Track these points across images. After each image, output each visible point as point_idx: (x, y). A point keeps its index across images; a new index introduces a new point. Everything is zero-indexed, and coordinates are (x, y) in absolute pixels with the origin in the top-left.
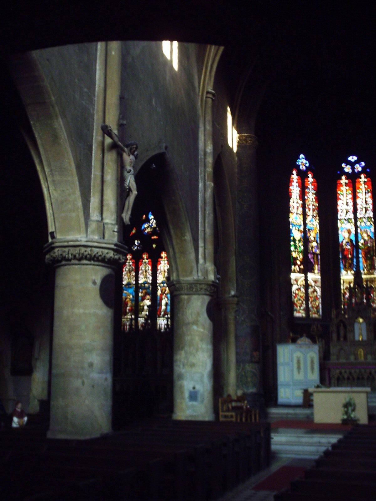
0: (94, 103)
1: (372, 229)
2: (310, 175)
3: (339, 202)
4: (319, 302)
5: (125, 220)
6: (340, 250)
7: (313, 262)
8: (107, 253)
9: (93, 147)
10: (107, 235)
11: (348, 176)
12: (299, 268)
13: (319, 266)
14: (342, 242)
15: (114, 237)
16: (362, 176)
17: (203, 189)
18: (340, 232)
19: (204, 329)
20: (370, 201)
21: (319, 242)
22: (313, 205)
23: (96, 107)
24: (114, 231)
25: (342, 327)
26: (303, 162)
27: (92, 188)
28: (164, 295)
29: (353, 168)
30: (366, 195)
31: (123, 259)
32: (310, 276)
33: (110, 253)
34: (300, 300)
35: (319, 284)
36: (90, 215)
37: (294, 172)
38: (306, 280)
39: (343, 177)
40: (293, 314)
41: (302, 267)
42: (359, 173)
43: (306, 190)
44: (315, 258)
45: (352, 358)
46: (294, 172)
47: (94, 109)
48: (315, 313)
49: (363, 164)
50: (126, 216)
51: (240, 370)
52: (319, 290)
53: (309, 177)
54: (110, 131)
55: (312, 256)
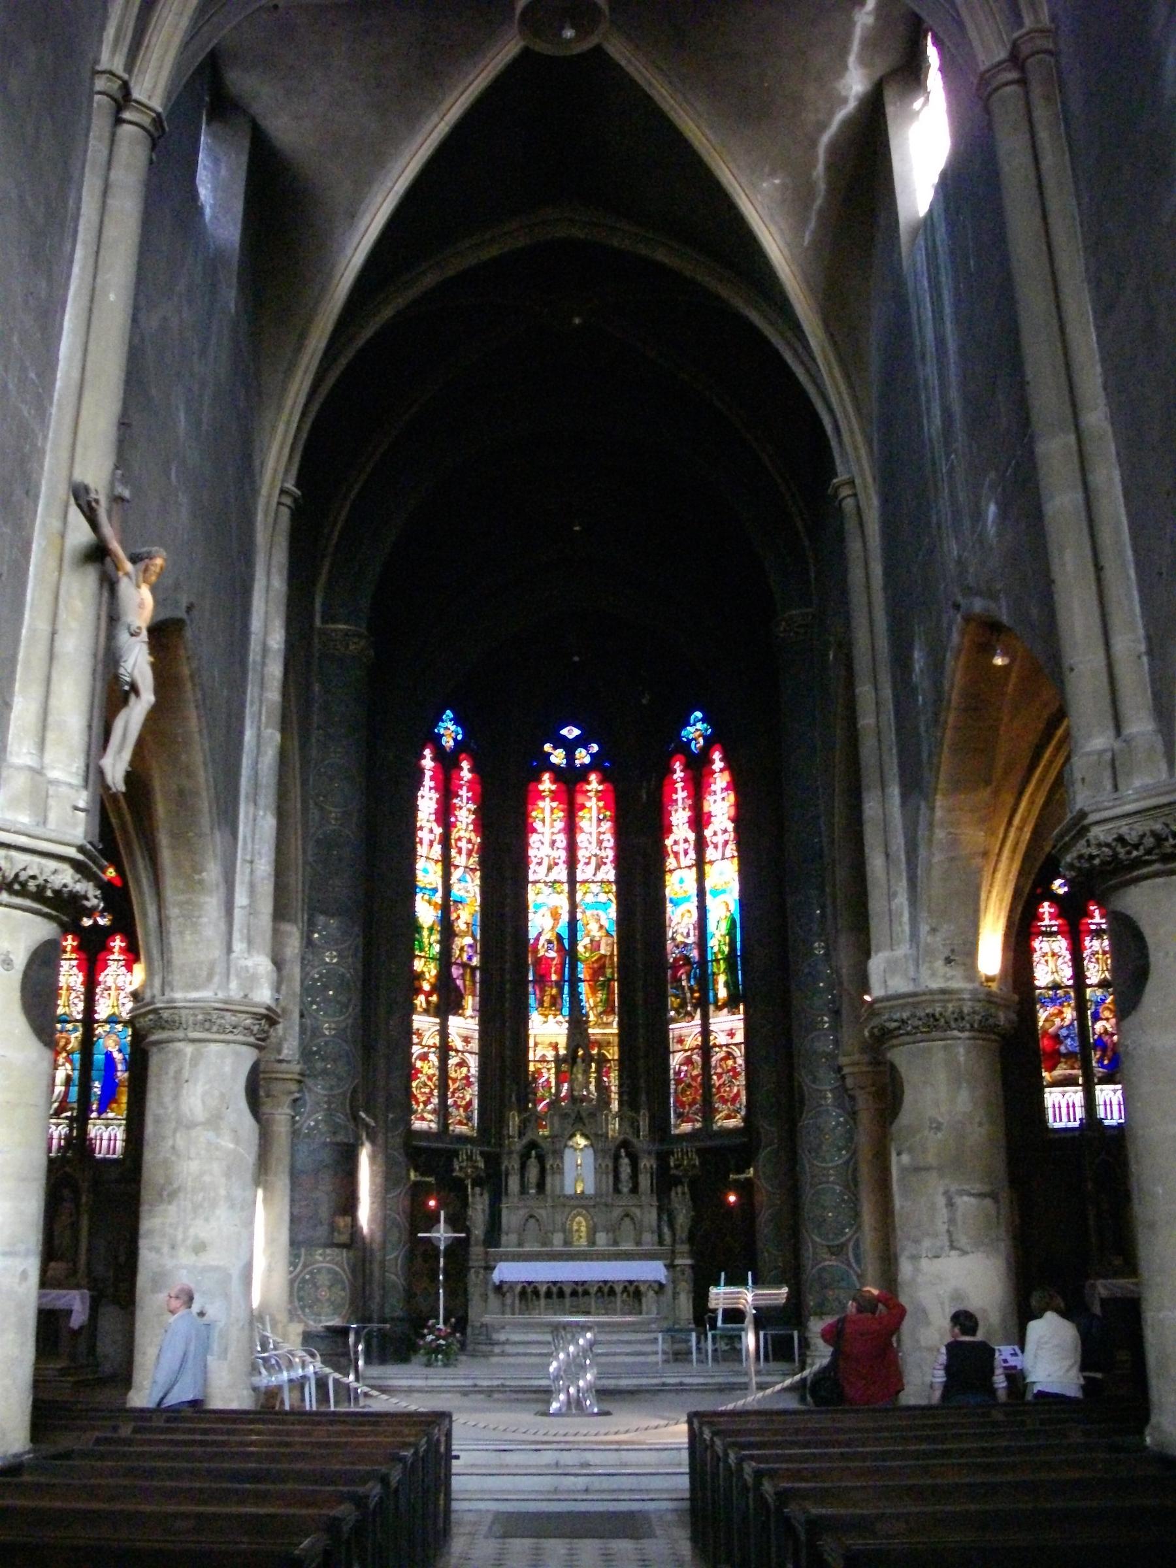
0: (49, 419)
1: (613, 909)
2: (465, 765)
3: (533, 839)
4: (472, 1094)
5: (109, 779)
6: (530, 961)
7: (462, 987)
8: (55, 872)
9: (34, 547)
10: (52, 816)
11: (558, 774)
12: (428, 1002)
13: (477, 999)
14: (537, 939)
15: (75, 825)
16: (593, 777)
17: (254, 743)
18: (531, 916)
19: (237, 1141)
20: (609, 840)
21: (478, 937)
22: (469, 841)
23: (51, 435)
24: (76, 808)
25: (533, 1162)
26: (449, 731)
27: (19, 668)
28: (64, 1055)
29: (570, 757)
30: (599, 826)
31: (96, 897)
32: (454, 1021)
33: (64, 870)
34: (425, 1085)
35: (475, 1046)
36: (9, 749)
37: (427, 752)
38: (444, 1033)
39: (546, 777)
40: (408, 1123)
41: (434, 998)
42: (586, 769)
43: (455, 801)
44: (468, 977)
45: (558, 1238)
46: (427, 752)
47: (45, 437)
48: (460, 1123)
49: (595, 748)
50: (116, 767)
51: (299, 1268)
52: (473, 1062)
53: (461, 769)
54: (94, 504)
55: (461, 971)
